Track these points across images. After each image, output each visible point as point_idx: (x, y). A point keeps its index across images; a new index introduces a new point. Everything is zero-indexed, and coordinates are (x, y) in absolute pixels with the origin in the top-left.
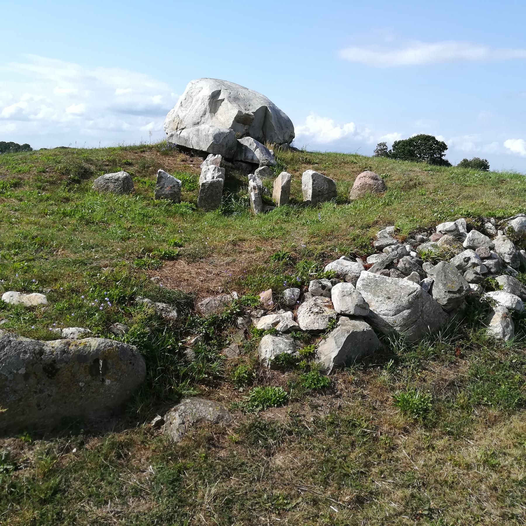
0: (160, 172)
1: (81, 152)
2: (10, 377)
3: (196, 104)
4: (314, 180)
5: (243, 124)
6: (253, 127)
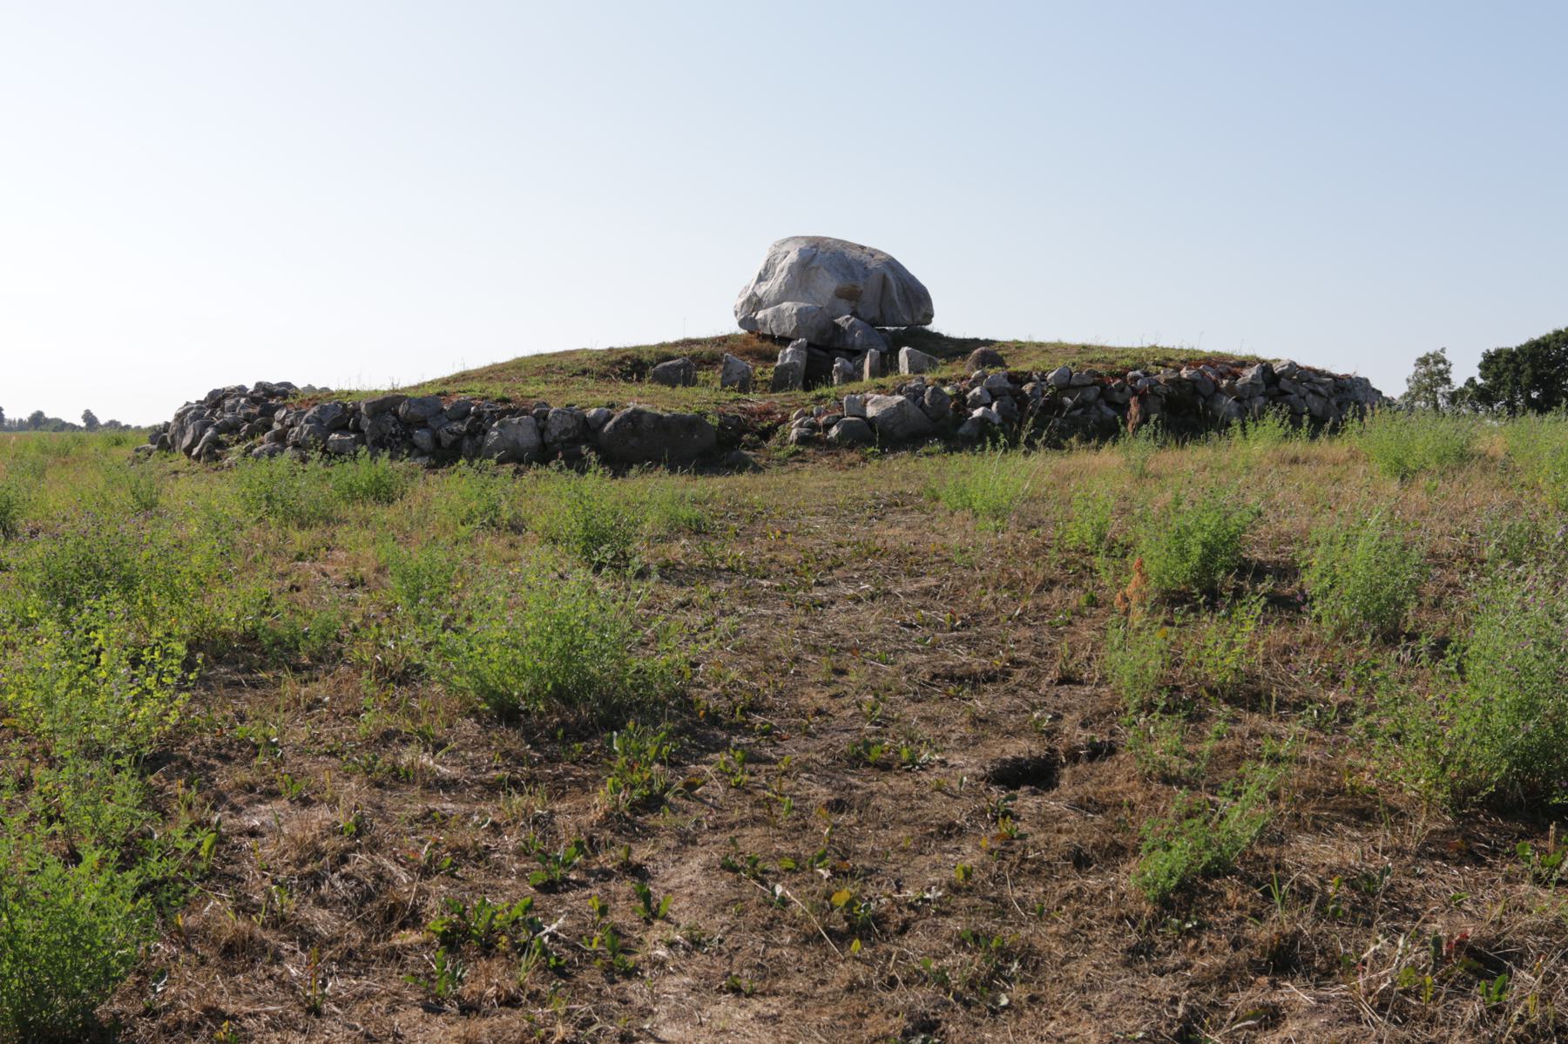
1: (627, 349)
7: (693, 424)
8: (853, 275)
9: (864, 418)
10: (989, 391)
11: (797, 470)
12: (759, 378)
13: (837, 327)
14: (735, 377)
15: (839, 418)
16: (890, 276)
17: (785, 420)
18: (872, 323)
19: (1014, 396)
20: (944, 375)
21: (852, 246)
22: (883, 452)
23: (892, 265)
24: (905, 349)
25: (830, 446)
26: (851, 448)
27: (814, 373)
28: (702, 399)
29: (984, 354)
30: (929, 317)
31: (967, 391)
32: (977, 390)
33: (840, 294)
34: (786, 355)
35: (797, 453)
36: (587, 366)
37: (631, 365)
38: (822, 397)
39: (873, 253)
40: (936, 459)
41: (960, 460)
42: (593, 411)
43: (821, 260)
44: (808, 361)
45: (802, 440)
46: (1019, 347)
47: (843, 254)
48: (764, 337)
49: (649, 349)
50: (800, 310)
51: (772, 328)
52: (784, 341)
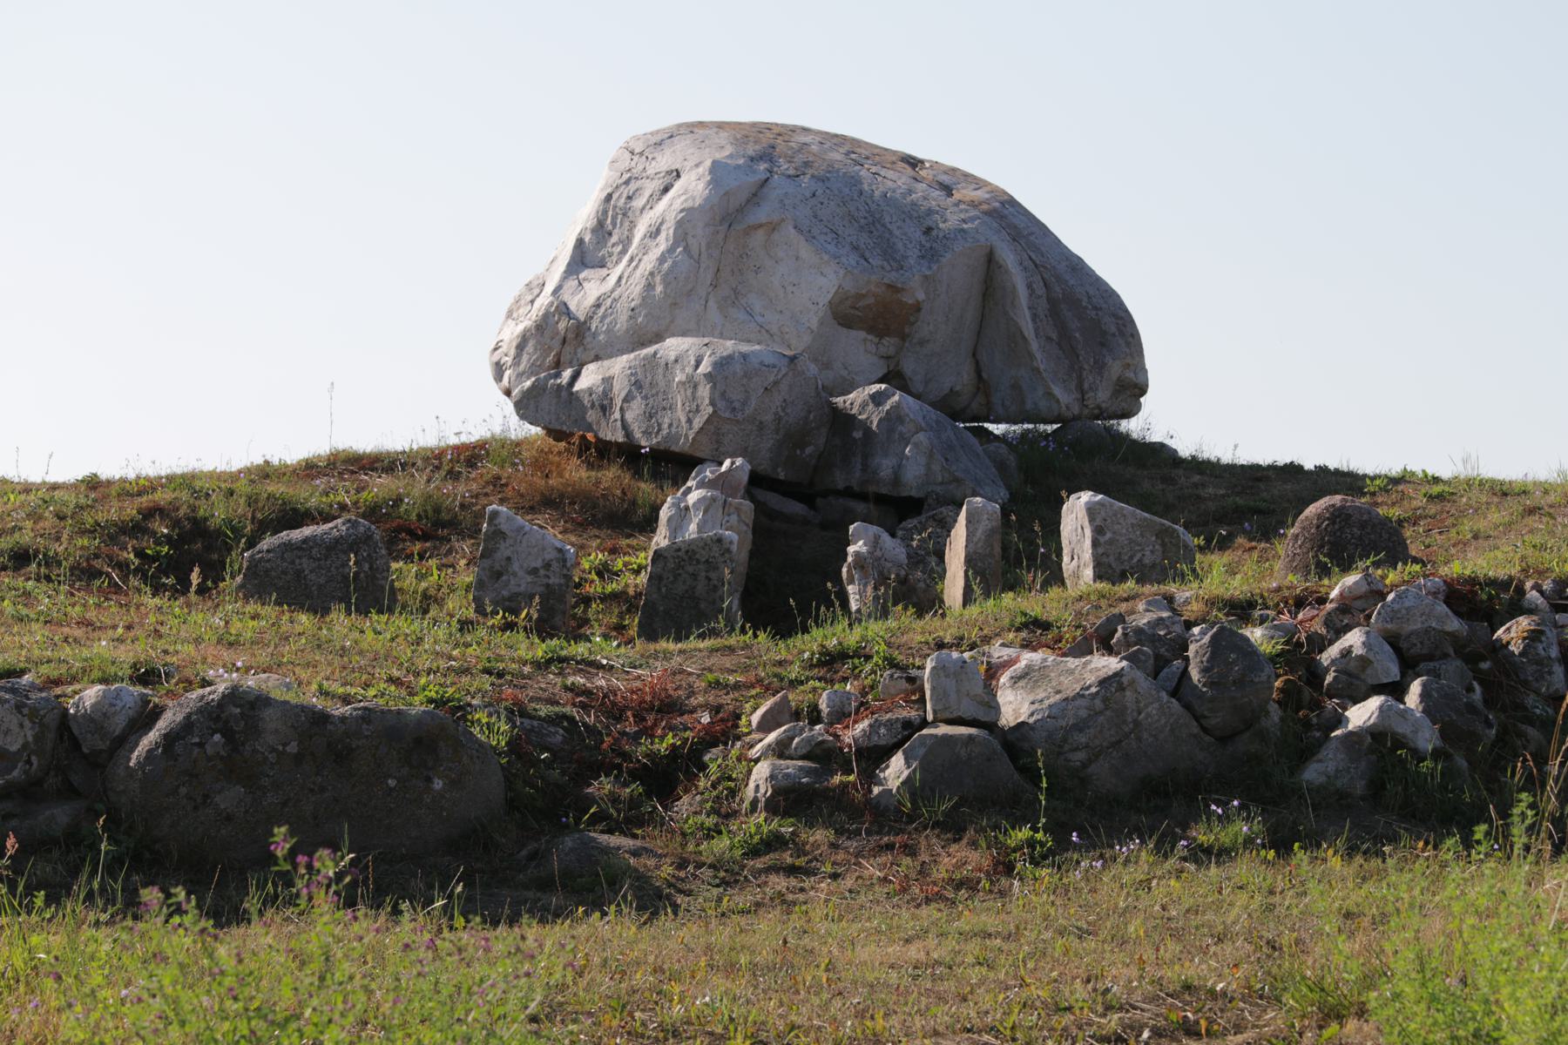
0: (495, 514)
1: (149, 486)
2: (272, 757)
3: (645, 250)
4: (1098, 531)
5: (871, 329)
6: (922, 343)
7: (431, 740)
8: (889, 252)
9: (991, 726)
10: (1393, 640)
11: (784, 903)
12: (595, 587)
13: (842, 422)
14: (520, 582)
15: (910, 727)
16: (1008, 257)
17: (725, 730)
18: (951, 408)
19: (1472, 659)
20: (1237, 587)
21: (878, 155)
22: (1063, 844)
23: (1009, 217)
24: (1086, 497)
25: (886, 823)
26: (953, 828)
27: (782, 582)
28: (413, 654)
29: (1337, 516)
30: (1132, 391)
31: (1321, 644)
32: (1354, 639)
33: (845, 314)
34: (689, 512)
35: (774, 843)
36: (26, 538)
37: (172, 538)
38: (841, 656)
39: (949, 181)
40: (1245, 869)
41: (1326, 881)
42: (91, 694)
43: (781, 197)
44: (757, 530)
45: (789, 800)
46: (1443, 496)
47: (855, 181)
48: (602, 452)
49: (226, 483)
50: (722, 364)
51: (629, 421)
52: (672, 465)
